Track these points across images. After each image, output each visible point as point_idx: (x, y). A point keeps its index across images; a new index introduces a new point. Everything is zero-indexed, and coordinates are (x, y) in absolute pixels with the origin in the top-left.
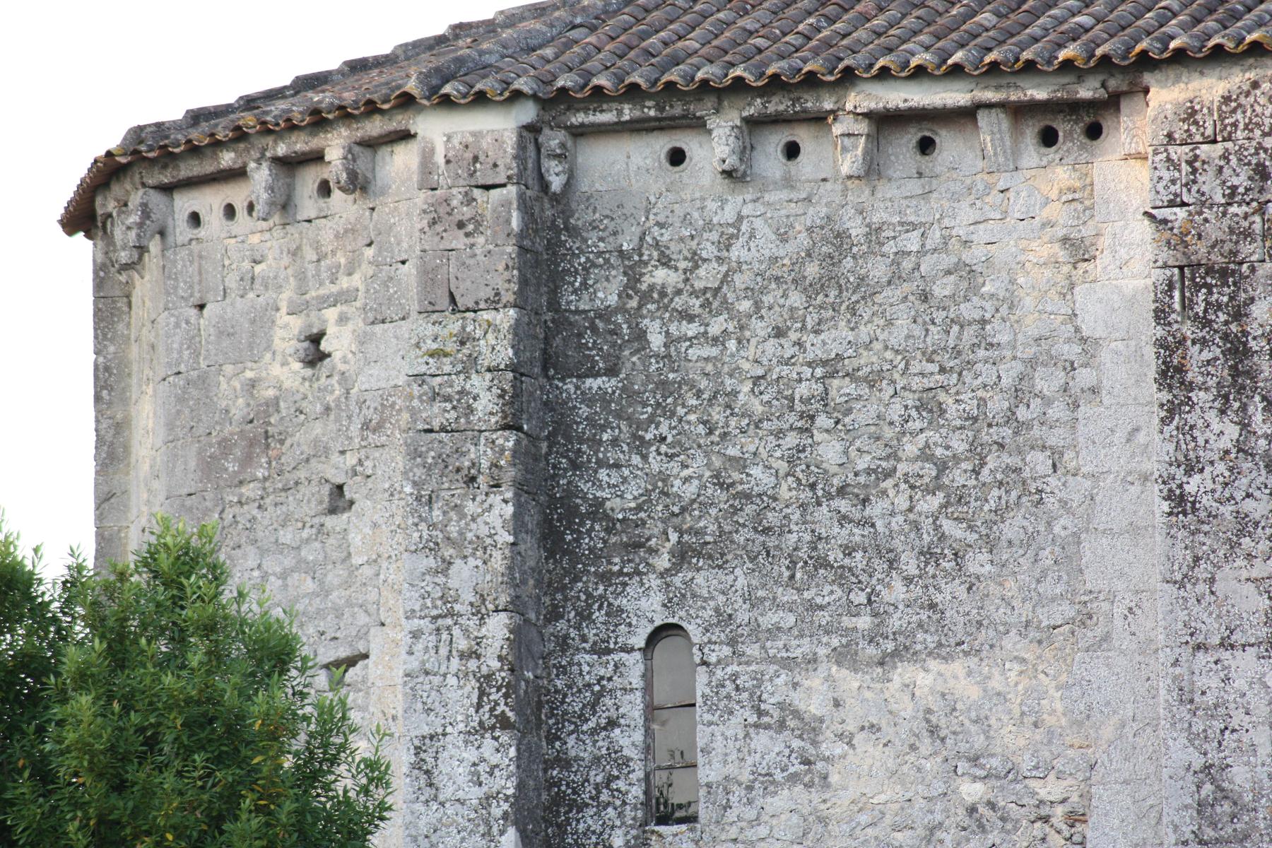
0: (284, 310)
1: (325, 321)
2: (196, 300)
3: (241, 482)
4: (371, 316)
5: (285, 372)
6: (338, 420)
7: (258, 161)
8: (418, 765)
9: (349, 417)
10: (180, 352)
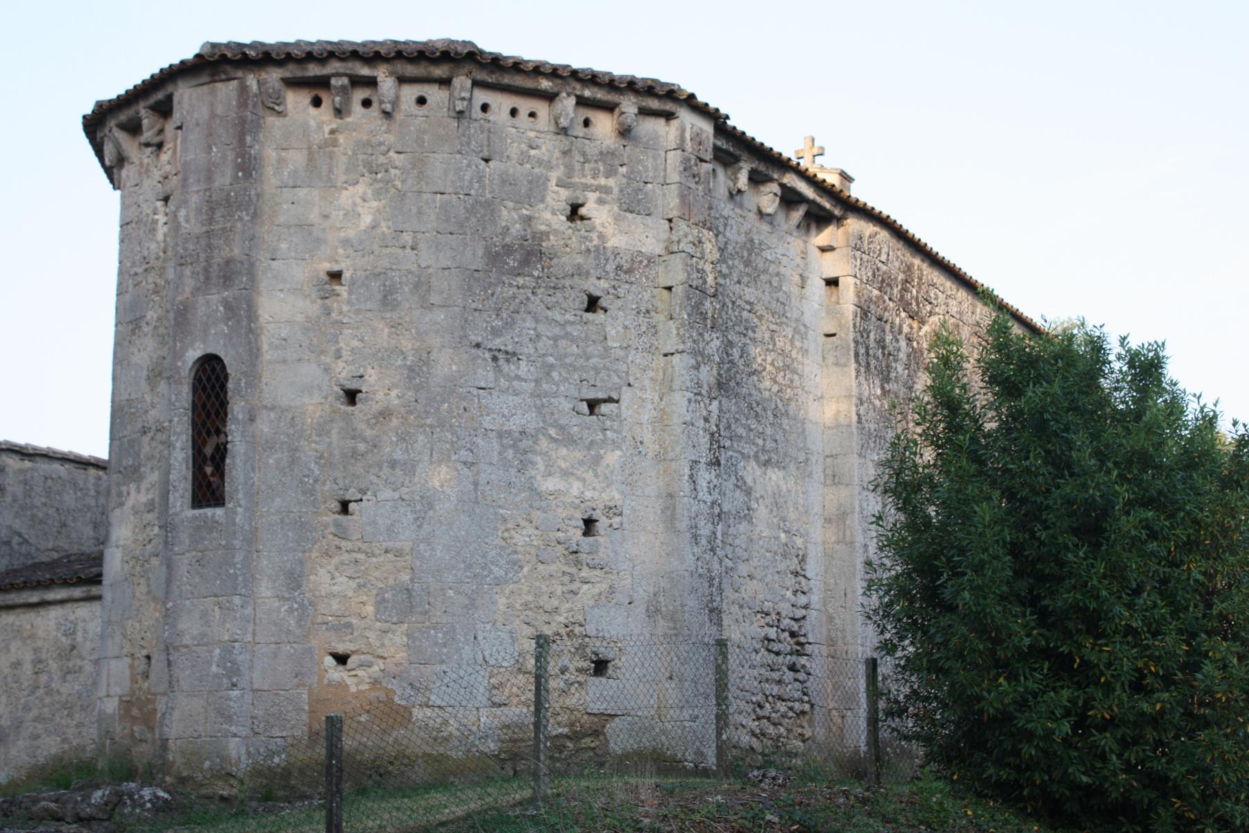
0: (554, 182)
1: (587, 199)
2: (486, 154)
3: (519, 274)
4: (625, 207)
5: (551, 217)
6: (597, 258)
7: (569, 95)
8: (691, 476)
9: (607, 260)
10: (471, 182)
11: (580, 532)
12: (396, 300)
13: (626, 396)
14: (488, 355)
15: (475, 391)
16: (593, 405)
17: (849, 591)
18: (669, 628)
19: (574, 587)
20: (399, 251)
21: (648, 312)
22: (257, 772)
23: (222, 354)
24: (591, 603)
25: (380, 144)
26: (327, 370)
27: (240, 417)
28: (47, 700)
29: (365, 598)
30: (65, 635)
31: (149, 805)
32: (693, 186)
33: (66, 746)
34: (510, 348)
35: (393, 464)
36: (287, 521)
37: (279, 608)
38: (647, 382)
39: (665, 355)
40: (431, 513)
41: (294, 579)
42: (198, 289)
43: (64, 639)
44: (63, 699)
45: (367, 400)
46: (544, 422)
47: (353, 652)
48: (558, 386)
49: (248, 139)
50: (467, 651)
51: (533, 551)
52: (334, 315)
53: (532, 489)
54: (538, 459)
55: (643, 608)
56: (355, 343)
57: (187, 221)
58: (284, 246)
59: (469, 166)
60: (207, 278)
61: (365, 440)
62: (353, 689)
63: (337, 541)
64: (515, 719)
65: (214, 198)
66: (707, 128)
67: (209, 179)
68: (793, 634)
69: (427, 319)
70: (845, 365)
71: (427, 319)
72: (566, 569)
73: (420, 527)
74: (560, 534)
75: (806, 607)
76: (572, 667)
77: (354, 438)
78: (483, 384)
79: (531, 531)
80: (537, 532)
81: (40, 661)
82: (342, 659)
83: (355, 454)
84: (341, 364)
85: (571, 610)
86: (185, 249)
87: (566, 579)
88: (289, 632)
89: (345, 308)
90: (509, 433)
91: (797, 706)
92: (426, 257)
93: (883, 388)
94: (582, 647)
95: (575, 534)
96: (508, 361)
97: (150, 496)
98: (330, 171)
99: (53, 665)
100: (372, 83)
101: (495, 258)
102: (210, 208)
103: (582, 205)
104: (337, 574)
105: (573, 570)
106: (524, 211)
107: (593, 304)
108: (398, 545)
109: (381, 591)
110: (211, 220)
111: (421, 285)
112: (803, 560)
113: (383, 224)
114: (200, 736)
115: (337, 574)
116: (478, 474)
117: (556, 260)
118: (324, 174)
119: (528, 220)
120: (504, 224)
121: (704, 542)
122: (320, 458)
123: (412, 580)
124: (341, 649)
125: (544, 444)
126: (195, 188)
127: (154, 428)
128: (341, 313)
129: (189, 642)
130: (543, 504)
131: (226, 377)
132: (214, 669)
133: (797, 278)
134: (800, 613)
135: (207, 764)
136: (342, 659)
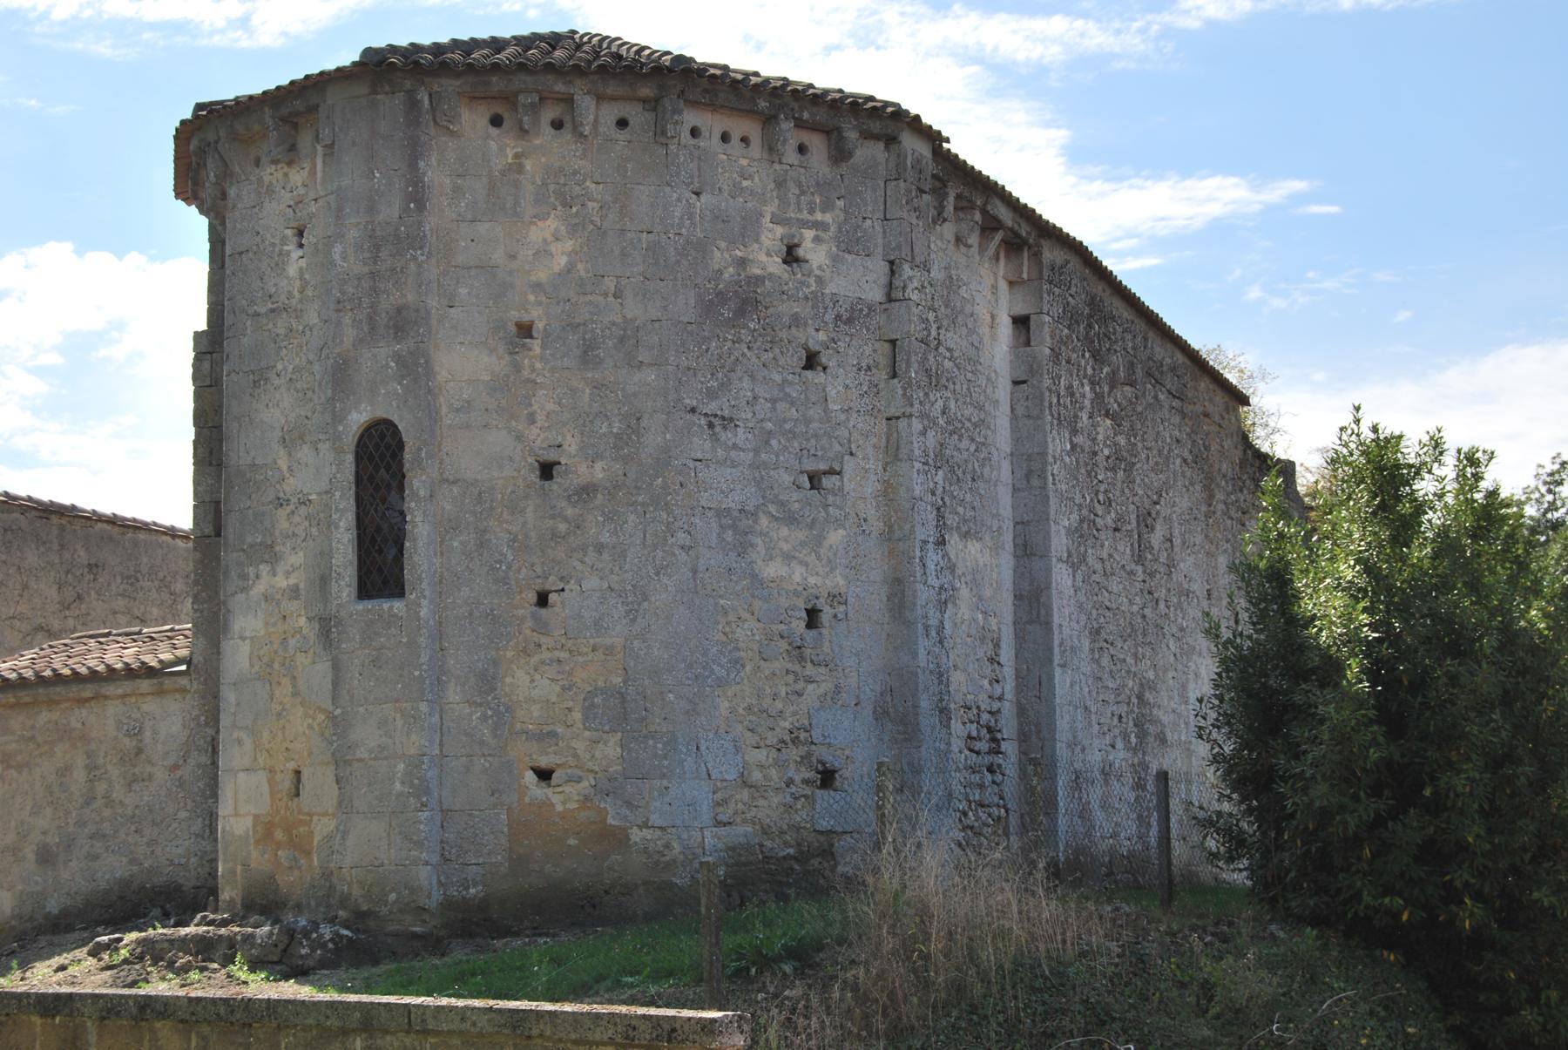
8: (921, 558)
10: (681, 218)
11: (803, 624)
12: (597, 356)
13: (849, 465)
14: (703, 422)
15: (691, 464)
16: (814, 479)
17: (1044, 677)
18: (899, 732)
19: (800, 685)
20: (601, 299)
21: (869, 368)
22: (448, 905)
23: (395, 419)
24: (817, 705)
25: (575, 173)
26: (519, 438)
27: (422, 493)
28: (107, 813)
29: (570, 704)
30: (128, 735)
31: (330, 945)
32: (914, 221)
33: (135, 868)
34: (726, 413)
35: (600, 548)
36: (476, 614)
37: (471, 714)
38: (870, 450)
39: (888, 419)
40: (646, 604)
41: (488, 681)
42: (362, 340)
43: (126, 740)
44: (129, 811)
45: (566, 472)
46: (764, 497)
47: (558, 765)
48: (777, 456)
49: (422, 164)
50: (689, 764)
51: (755, 647)
52: (526, 373)
53: (754, 576)
54: (758, 541)
55: (870, 710)
56: (551, 406)
57: (344, 259)
58: (463, 291)
59: (679, 200)
60: (373, 328)
61: (566, 519)
62: (559, 808)
63: (536, 637)
64: (741, 839)
65: (378, 233)
66: (925, 150)
67: (372, 209)
68: (990, 730)
69: (636, 379)
70: (1038, 418)
71: (636, 379)
72: (789, 666)
73: (633, 621)
74: (782, 627)
75: (1000, 699)
76: (797, 779)
77: (553, 517)
78: (699, 456)
79: (752, 623)
80: (761, 625)
81: (96, 768)
82: (544, 775)
83: (554, 535)
84: (535, 431)
85: (795, 713)
86: (343, 293)
87: (791, 678)
88: (482, 743)
89: (538, 365)
90: (728, 510)
91: (995, 811)
92: (634, 309)
93: (1071, 442)
94: (809, 754)
95: (799, 625)
96: (725, 428)
97: (292, 581)
98: (517, 203)
99: (114, 772)
100: (569, 100)
101: (709, 308)
102: (375, 245)
103: (798, 245)
104: (538, 676)
105: (797, 668)
106: (739, 253)
107: (811, 361)
108: (608, 641)
109: (590, 695)
110: (376, 259)
111: (629, 337)
112: (997, 645)
113: (580, 266)
114: (382, 865)
115: (538, 676)
116: (697, 558)
117: (771, 310)
118: (508, 206)
119: (742, 263)
120: (716, 267)
121: (933, 633)
122: (514, 541)
123: (625, 682)
124: (544, 762)
125: (764, 521)
126: (354, 221)
127: (294, 500)
128: (533, 371)
129: (365, 756)
130: (765, 592)
131: (401, 445)
132: (398, 786)
133: (988, 317)
134: (996, 705)
135: (393, 896)
136: (544, 775)
